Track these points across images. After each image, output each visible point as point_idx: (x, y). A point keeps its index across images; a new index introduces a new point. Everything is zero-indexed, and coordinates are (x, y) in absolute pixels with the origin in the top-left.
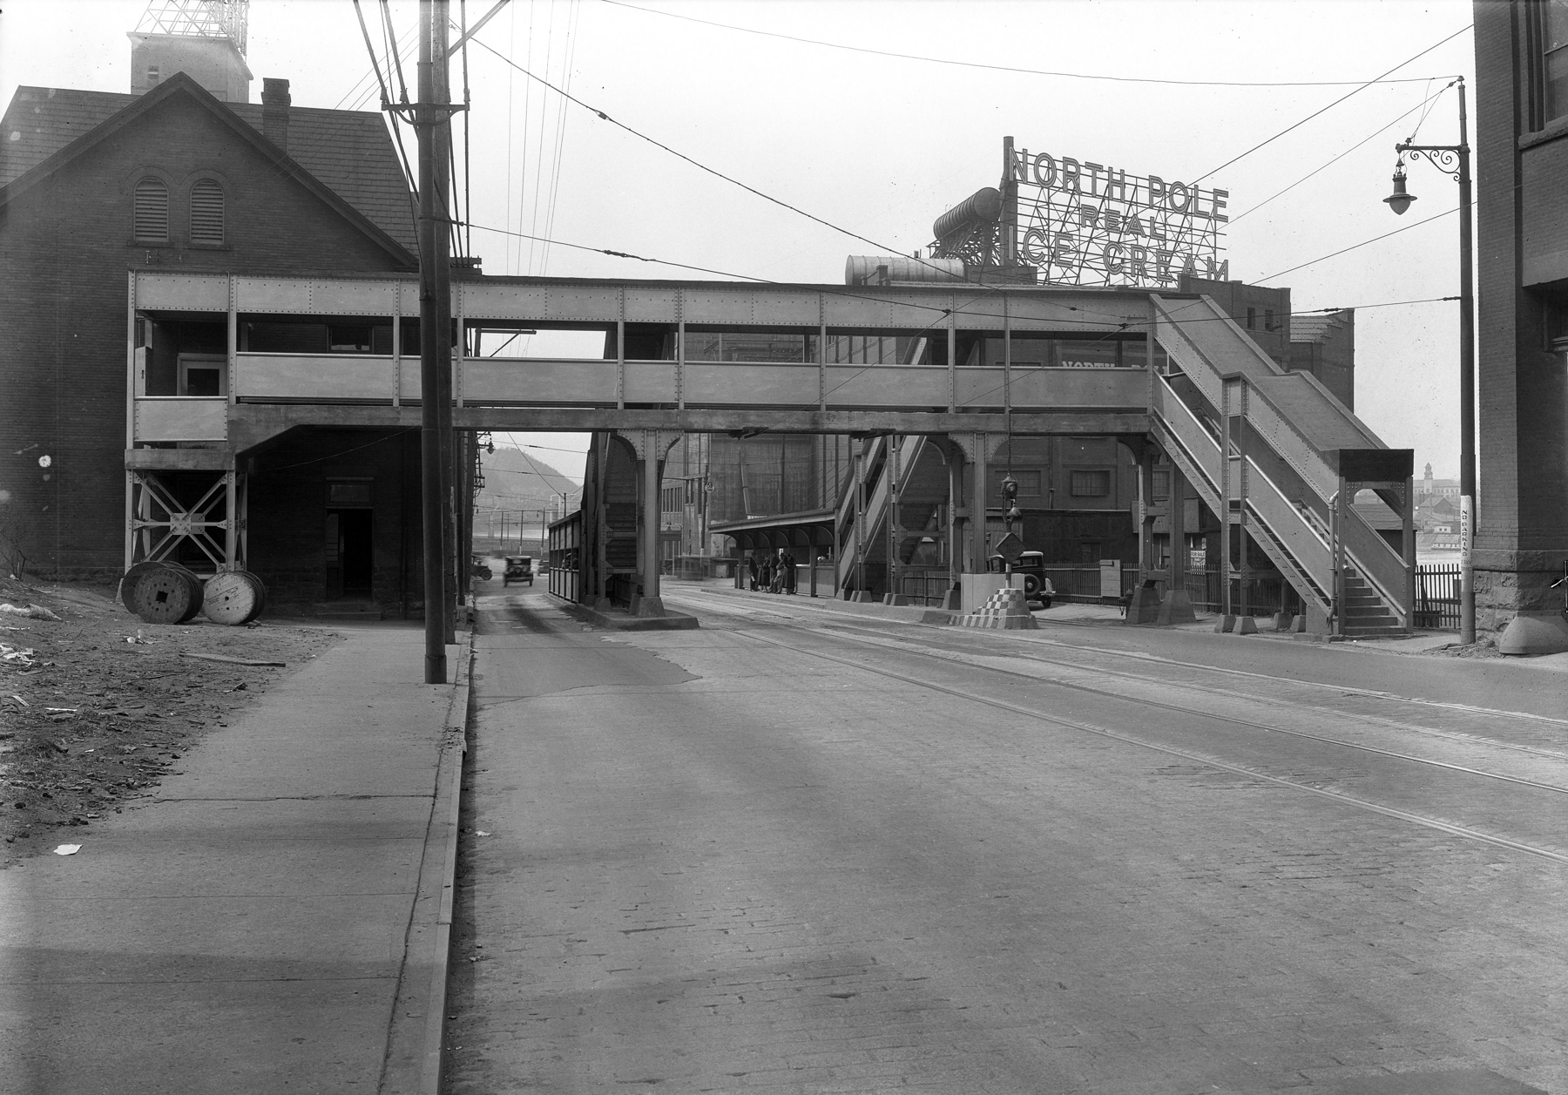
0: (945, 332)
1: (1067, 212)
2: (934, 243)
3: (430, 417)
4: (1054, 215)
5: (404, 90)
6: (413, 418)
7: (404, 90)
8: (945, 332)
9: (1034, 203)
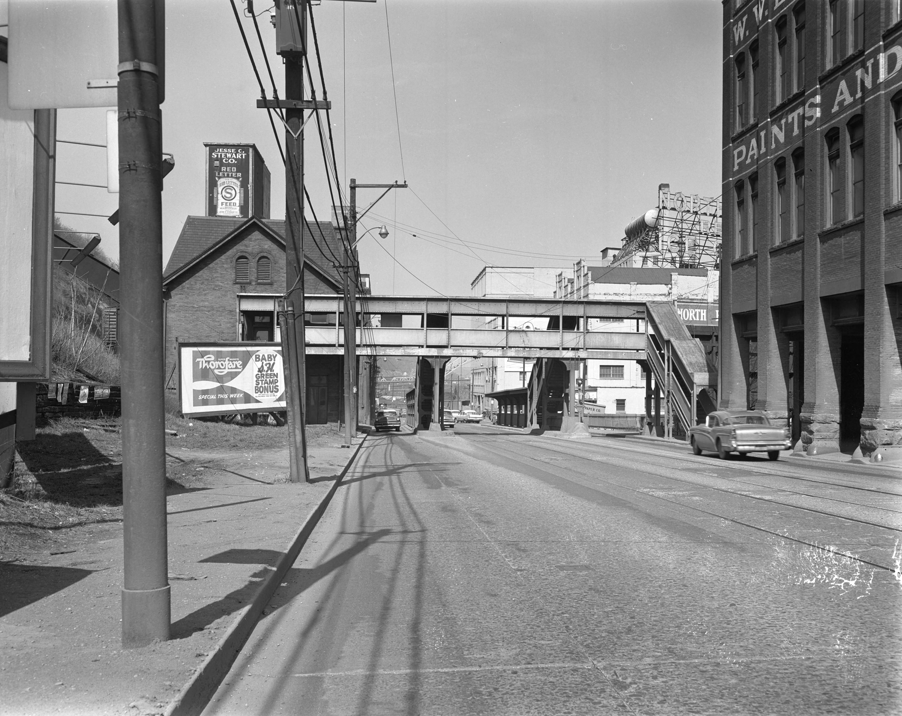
0: (558, 317)
1: (693, 224)
2: (625, 238)
3: (347, 351)
4: (685, 226)
5: (275, 91)
6: (341, 352)
7: (275, 91)
8: (558, 317)
9: (674, 220)
